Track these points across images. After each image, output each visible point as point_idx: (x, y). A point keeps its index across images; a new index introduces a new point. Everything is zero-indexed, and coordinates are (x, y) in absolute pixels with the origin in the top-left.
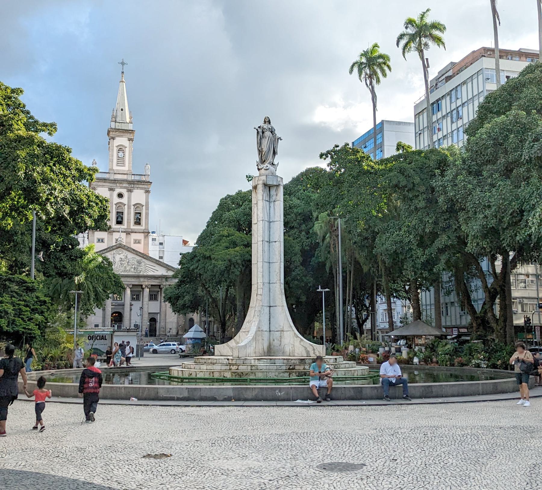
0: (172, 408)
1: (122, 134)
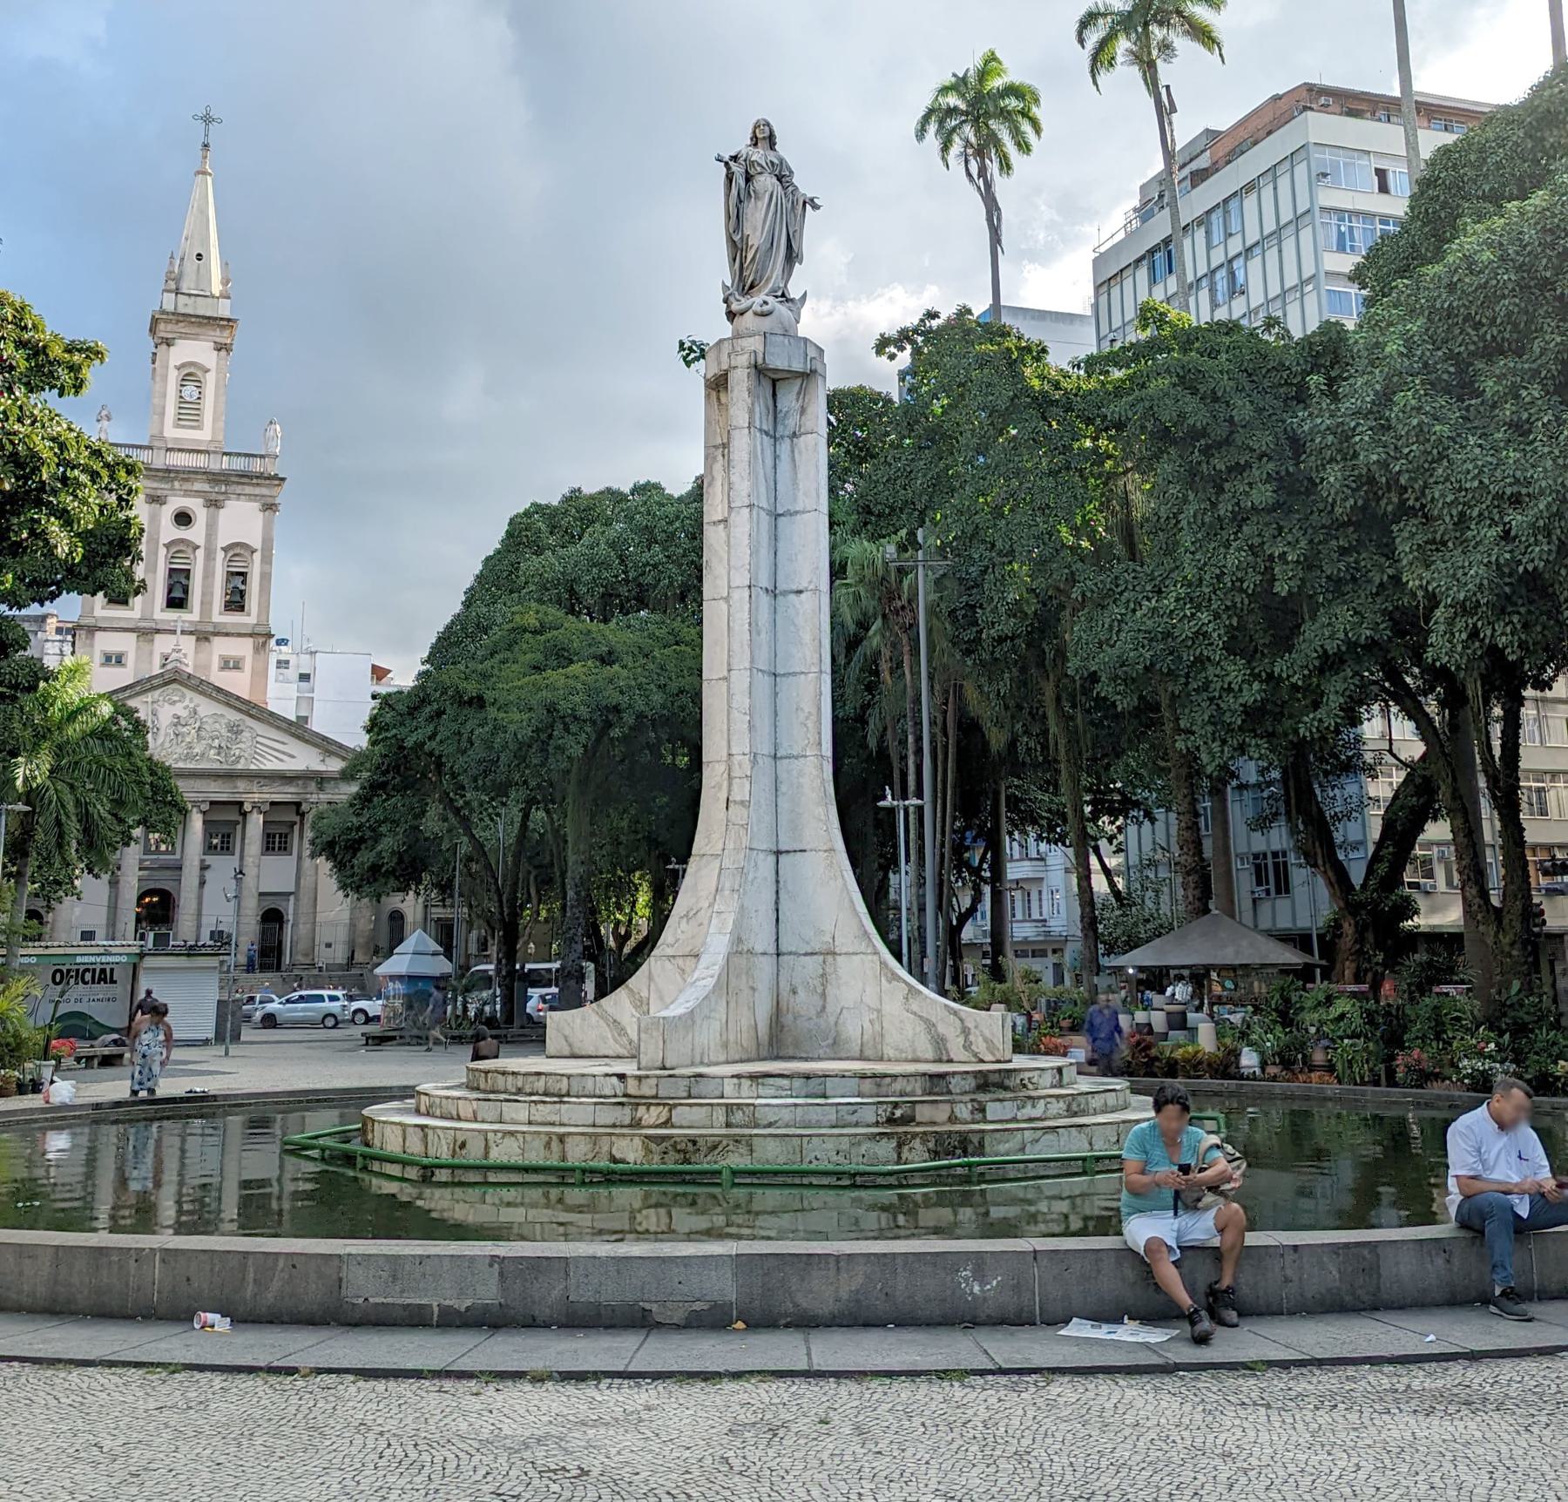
0: (428, 1396)
1: (195, 330)
